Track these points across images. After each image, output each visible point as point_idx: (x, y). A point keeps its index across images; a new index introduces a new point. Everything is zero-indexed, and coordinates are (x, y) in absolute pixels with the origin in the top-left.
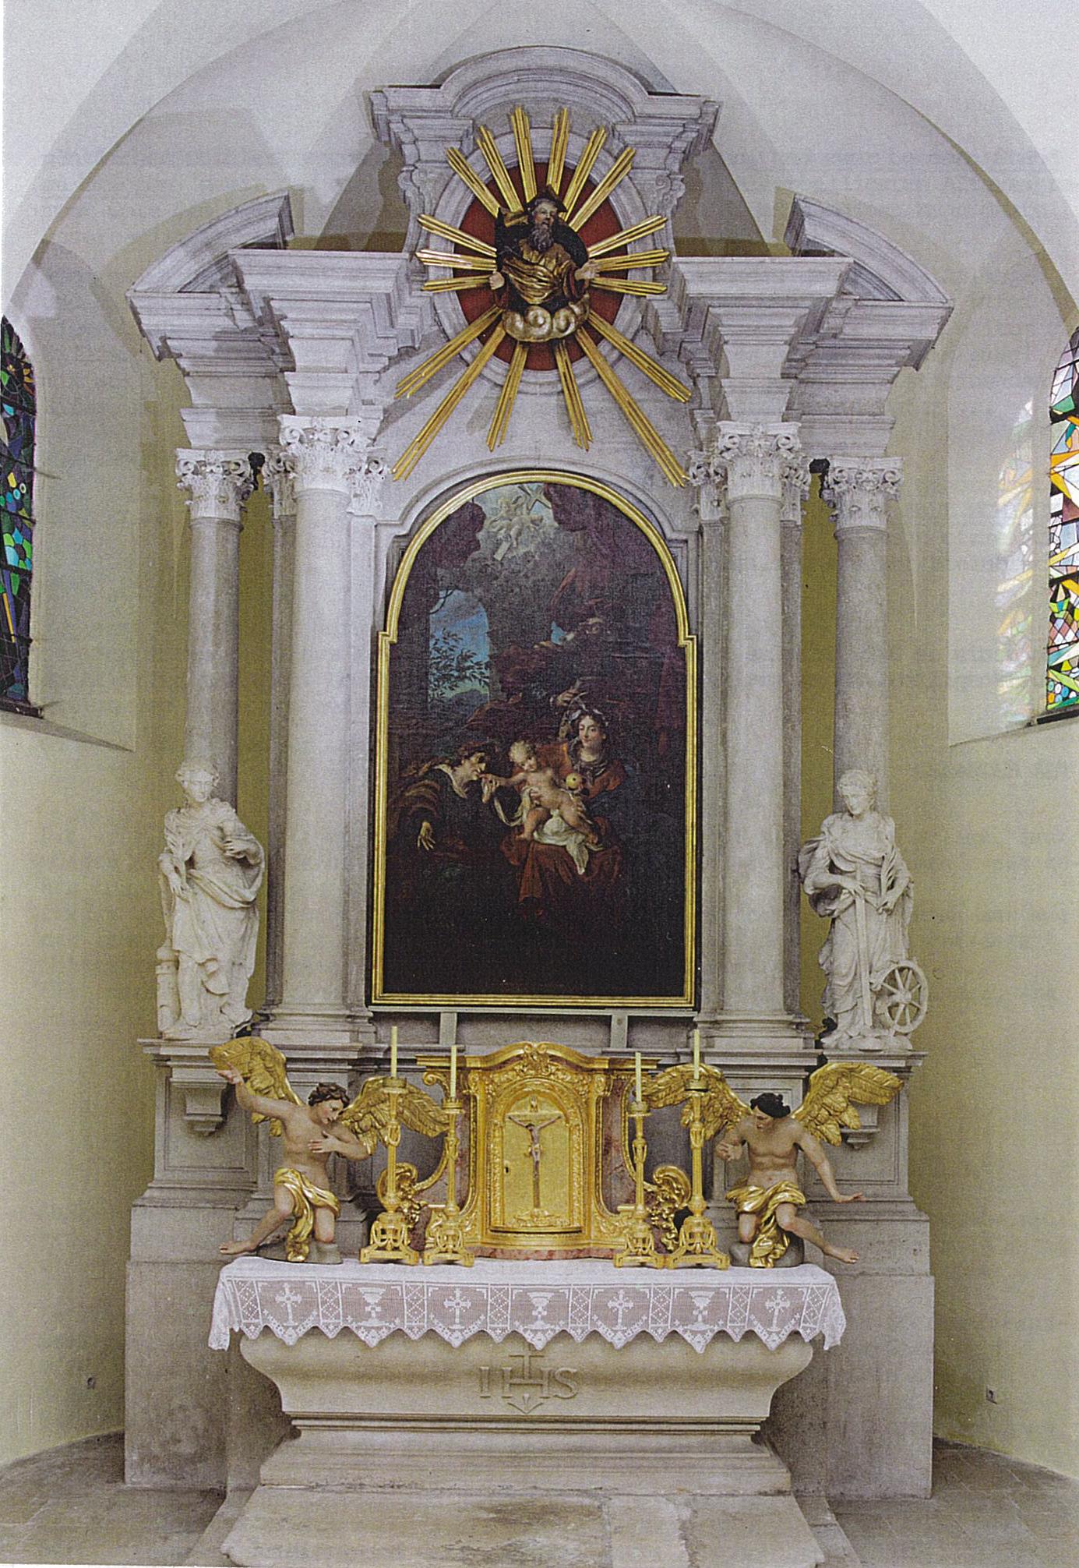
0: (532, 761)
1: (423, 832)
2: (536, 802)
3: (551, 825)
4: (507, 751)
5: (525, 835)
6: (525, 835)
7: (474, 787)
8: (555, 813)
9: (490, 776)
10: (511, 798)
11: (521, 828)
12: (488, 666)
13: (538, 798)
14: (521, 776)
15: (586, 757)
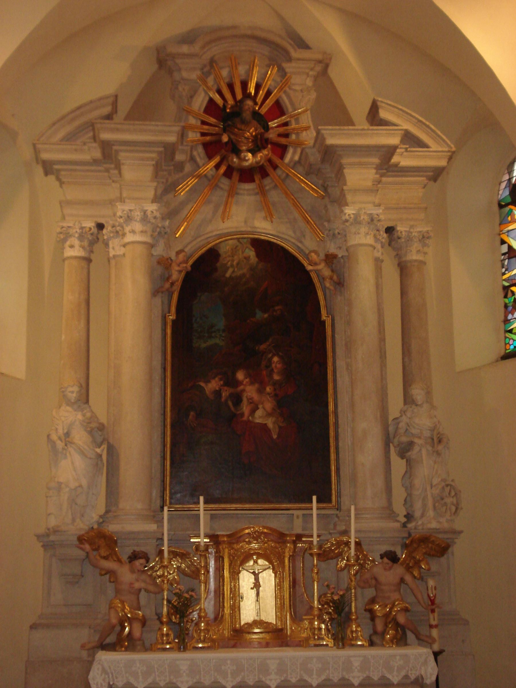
0: (247, 380)
1: (190, 417)
2: (251, 401)
3: (259, 413)
4: (234, 374)
5: (245, 418)
6: (245, 418)
7: (218, 393)
8: (260, 406)
9: (226, 388)
10: (237, 399)
11: (242, 415)
12: (224, 331)
13: (251, 399)
14: (242, 387)
15: (276, 377)
